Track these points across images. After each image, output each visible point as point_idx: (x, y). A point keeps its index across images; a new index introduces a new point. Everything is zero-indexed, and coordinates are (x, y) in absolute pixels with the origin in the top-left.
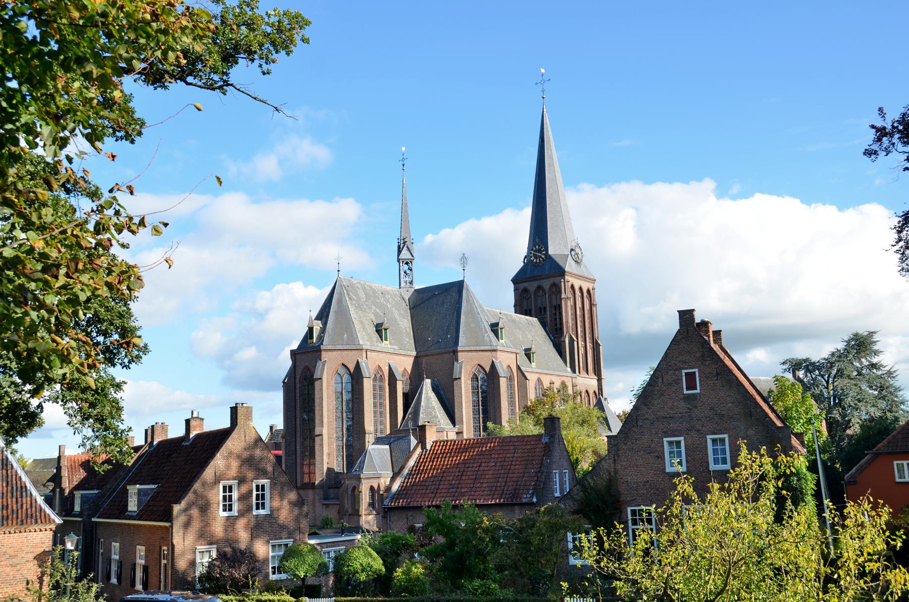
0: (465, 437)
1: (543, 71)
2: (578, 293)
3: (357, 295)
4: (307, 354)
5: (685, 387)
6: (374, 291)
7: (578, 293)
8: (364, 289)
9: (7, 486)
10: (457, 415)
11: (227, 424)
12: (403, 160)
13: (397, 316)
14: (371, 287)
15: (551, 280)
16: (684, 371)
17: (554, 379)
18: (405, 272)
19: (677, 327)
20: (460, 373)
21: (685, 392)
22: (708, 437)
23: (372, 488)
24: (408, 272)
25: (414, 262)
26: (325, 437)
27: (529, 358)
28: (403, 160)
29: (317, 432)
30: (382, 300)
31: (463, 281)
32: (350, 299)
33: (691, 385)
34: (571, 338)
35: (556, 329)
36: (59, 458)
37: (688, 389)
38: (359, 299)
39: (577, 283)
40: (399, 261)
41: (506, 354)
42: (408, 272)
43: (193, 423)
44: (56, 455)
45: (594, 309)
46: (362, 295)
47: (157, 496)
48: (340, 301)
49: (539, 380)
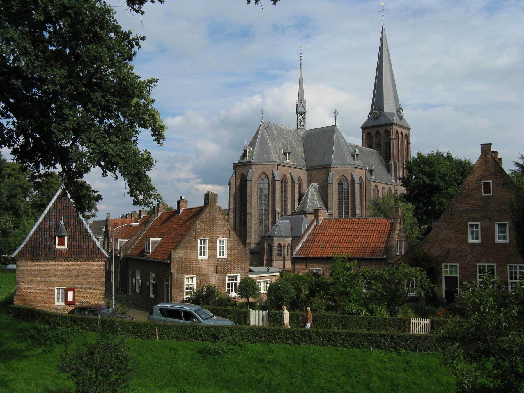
0: (334, 217)
1: (382, 4)
2: (400, 136)
3: (272, 132)
4: (242, 167)
5: (483, 191)
6: (282, 130)
7: (400, 136)
8: (276, 129)
9: (81, 235)
10: (329, 205)
11: (203, 204)
12: (301, 54)
13: (295, 145)
14: (280, 128)
15: (385, 128)
16: (483, 182)
17: (385, 186)
18: (300, 120)
19: (480, 154)
20: (332, 180)
21: (483, 194)
22: (496, 222)
23: (280, 245)
24: (302, 120)
25: (306, 114)
26: (253, 214)
27: (371, 173)
28: (301, 54)
29: (248, 210)
30: (287, 136)
31: (335, 126)
32: (269, 134)
33: (487, 190)
34: (395, 162)
35: (387, 157)
36: (107, 220)
37: (59, 245)
38: (274, 135)
39: (400, 130)
40: (297, 113)
41: (359, 170)
42: (302, 120)
43: (181, 203)
44: (105, 219)
45: (409, 145)
46: (275, 133)
47: (21, 241)
48: (262, 136)
49: (376, 185)
